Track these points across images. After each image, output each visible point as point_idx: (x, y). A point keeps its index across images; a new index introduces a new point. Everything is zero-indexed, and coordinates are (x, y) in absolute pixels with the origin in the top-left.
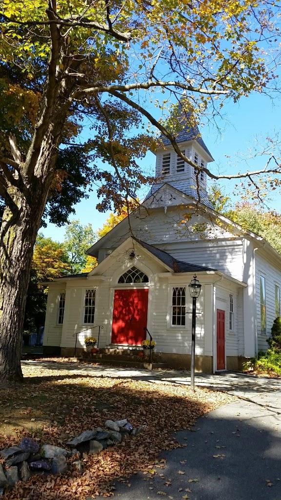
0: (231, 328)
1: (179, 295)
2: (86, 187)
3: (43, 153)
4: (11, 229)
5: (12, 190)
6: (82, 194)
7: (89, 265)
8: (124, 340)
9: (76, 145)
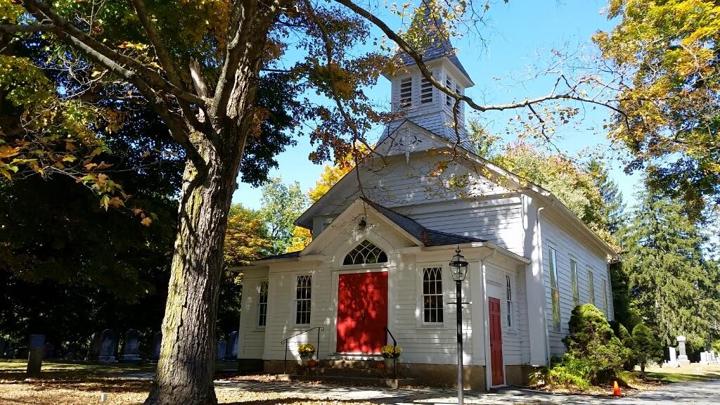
1: (432, 278)
2: (294, 129)
3: (238, 84)
4: (196, 192)
5: (196, 137)
6: (286, 140)
7: (299, 241)
8: (355, 347)
9: (279, 71)
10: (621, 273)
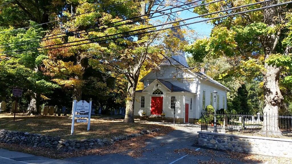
0: (191, 109)
4: (131, 88)
10: (246, 90)
